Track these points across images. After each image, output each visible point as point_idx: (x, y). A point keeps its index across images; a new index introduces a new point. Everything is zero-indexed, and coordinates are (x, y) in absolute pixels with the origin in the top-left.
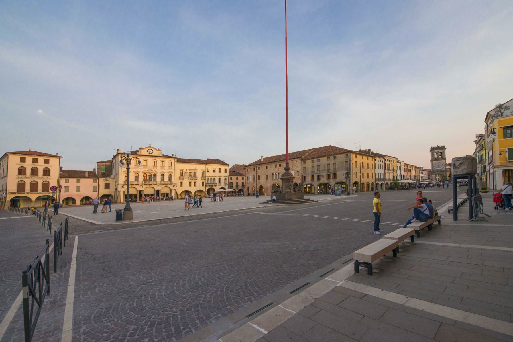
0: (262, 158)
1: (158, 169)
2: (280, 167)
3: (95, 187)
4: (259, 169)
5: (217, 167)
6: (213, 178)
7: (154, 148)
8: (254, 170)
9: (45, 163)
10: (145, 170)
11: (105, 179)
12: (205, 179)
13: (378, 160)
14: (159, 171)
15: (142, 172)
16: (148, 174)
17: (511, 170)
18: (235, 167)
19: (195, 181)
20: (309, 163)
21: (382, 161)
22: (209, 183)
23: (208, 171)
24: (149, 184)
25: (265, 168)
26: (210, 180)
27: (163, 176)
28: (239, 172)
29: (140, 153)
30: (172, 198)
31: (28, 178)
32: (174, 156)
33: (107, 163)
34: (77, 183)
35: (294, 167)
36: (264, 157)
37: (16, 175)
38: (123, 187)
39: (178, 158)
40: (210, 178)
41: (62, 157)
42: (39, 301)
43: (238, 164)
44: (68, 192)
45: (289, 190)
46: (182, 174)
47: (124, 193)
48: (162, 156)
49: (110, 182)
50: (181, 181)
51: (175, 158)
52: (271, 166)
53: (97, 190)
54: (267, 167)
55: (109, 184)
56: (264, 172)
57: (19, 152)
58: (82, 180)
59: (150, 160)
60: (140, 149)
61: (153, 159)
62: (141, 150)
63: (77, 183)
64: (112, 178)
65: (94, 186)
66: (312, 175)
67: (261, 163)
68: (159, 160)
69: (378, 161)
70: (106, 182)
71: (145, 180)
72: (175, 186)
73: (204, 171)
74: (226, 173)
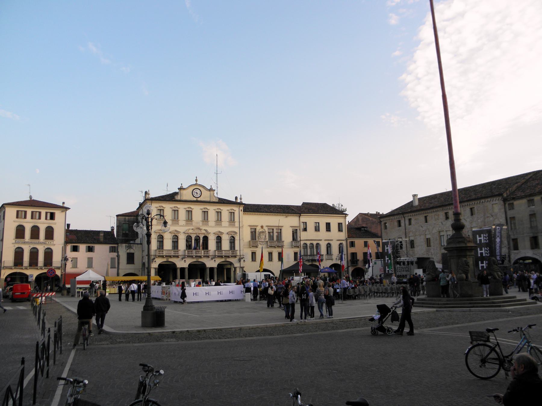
0: (414, 198)
1: (211, 227)
2: (410, 226)
3: (112, 259)
4: (410, 224)
5: (323, 220)
6: (315, 243)
7: (203, 187)
8: (400, 225)
11: (127, 245)
12: (298, 247)
14: (212, 230)
18: (360, 218)
20: (521, 205)
22: (307, 255)
23: (305, 230)
24: (196, 256)
25: (423, 219)
26: (308, 247)
27: (219, 240)
28: (369, 230)
29: (181, 196)
31: (27, 243)
32: (239, 201)
33: (131, 216)
35: (488, 217)
36: (419, 197)
37: (13, 238)
38: (154, 261)
39: (245, 204)
40: (308, 243)
41: (70, 209)
42: (10, 393)
43: (366, 212)
44: (76, 267)
45: (464, 276)
46: (253, 234)
48: (217, 201)
49: (134, 251)
51: (241, 204)
52: (436, 217)
53: (117, 266)
54: (426, 217)
55: (133, 254)
56: (421, 228)
59: (197, 210)
60: (180, 189)
61: (202, 207)
62: (182, 191)
64: (138, 244)
65: (111, 258)
66: (531, 235)
67: (415, 209)
68: (212, 210)
70: (128, 251)
71: (189, 247)
72: (242, 260)
73: (297, 230)
74: (341, 233)
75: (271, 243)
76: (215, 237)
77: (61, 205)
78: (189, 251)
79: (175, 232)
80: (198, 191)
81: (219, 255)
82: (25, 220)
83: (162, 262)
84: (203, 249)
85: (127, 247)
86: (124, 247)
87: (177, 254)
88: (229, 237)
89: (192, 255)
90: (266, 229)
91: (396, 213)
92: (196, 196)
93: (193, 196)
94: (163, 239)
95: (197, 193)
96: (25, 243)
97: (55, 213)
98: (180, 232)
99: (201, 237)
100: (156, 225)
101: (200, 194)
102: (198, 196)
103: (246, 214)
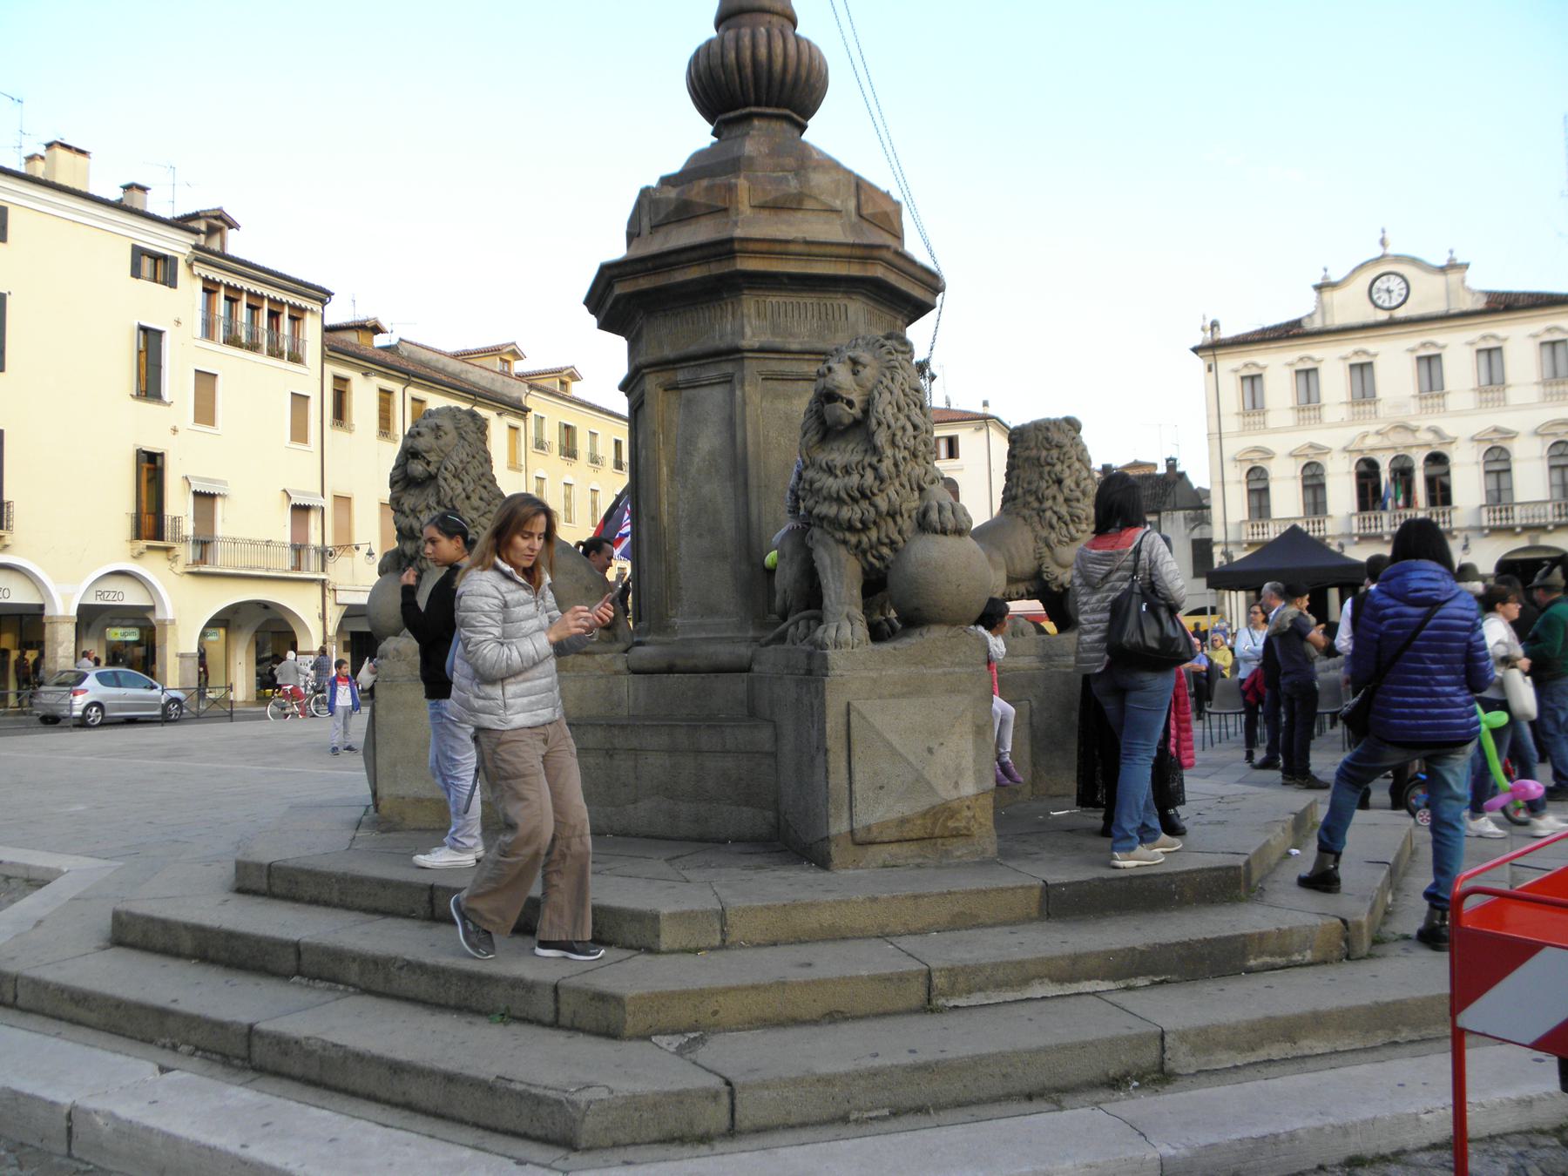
1: (1459, 414)
7: (1414, 261)
9: (292, 440)
15: (1345, 450)
17: (1563, 341)
27: (1498, 464)
30: (989, 627)
57: (1264, 331)
70: (1196, 534)
76: (1478, 454)
77: (980, 410)
78: (1364, 519)
79: (1310, 452)
80: (1395, 284)
81: (1256, 537)
83: (1509, 550)
85: (1193, 520)
86: (1182, 519)
87: (1319, 531)
88: (1351, 461)
89: (1379, 530)
92: (1386, 305)
94: (1510, 464)
95: (1389, 291)
97: (957, 437)
98: (1330, 449)
99: (1418, 459)
100: (1240, 434)
102: (1396, 300)
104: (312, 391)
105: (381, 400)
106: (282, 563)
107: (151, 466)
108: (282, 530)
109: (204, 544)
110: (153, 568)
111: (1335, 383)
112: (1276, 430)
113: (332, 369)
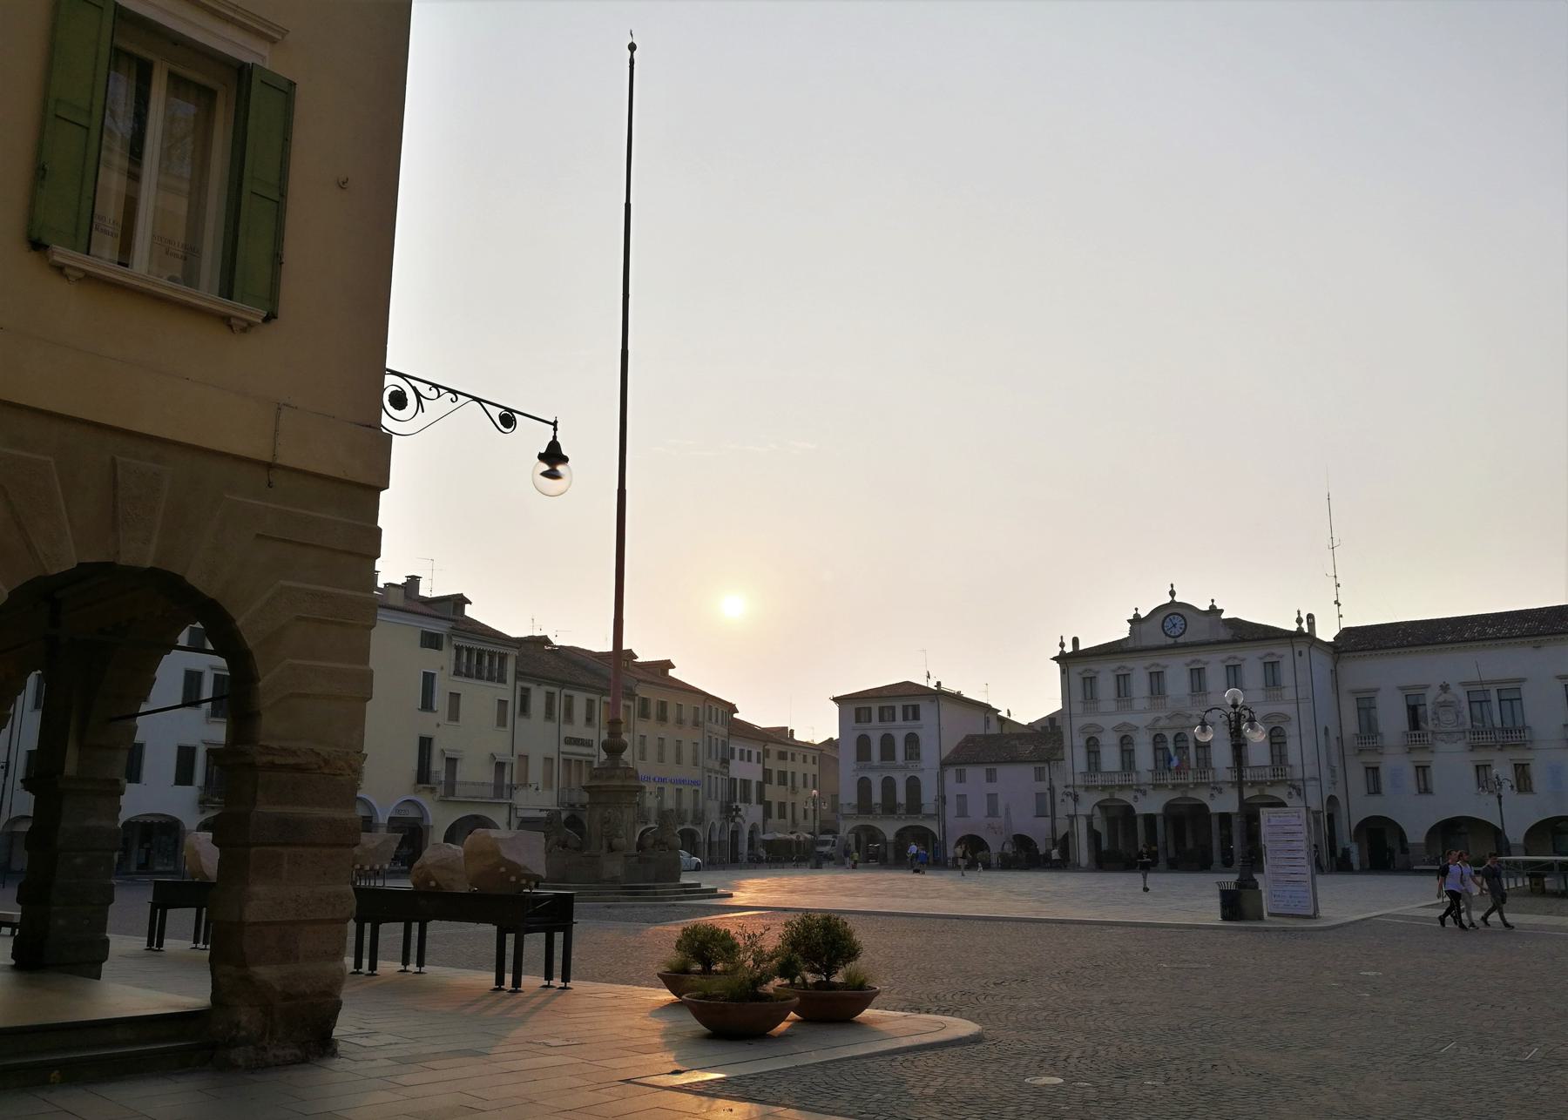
10: (1156, 715)
13: (805, 756)
16: (1170, 736)
19: (1519, 756)
21: (810, 760)
27: (1126, 746)
34: (987, 781)
47: (1090, 826)
50: (1422, 758)
58: (1003, 771)
63: (987, 781)
69: (805, 761)
75: (1476, 736)
80: (1178, 620)
82: (893, 723)
84: (779, 784)
90: (1460, 693)
91: (885, 693)
93: (1164, 635)
96: (872, 769)
101: (1183, 626)
103: (1411, 651)
104: (508, 696)
105: (547, 697)
106: (489, 792)
107: (425, 744)
108: (489, 777)
109: (451, 785)
110: (426, 800)
111: (1140, 685)
112: (1104, 714)
113: (520, 684)
